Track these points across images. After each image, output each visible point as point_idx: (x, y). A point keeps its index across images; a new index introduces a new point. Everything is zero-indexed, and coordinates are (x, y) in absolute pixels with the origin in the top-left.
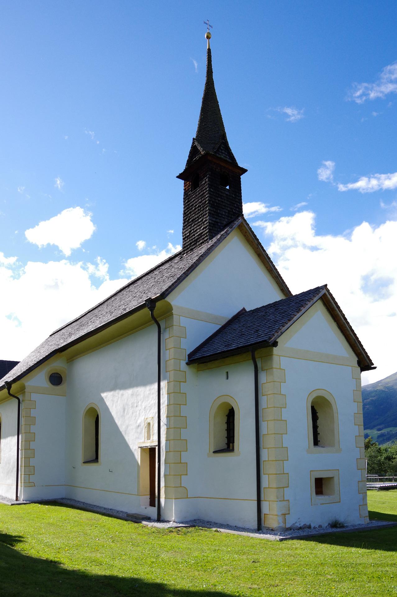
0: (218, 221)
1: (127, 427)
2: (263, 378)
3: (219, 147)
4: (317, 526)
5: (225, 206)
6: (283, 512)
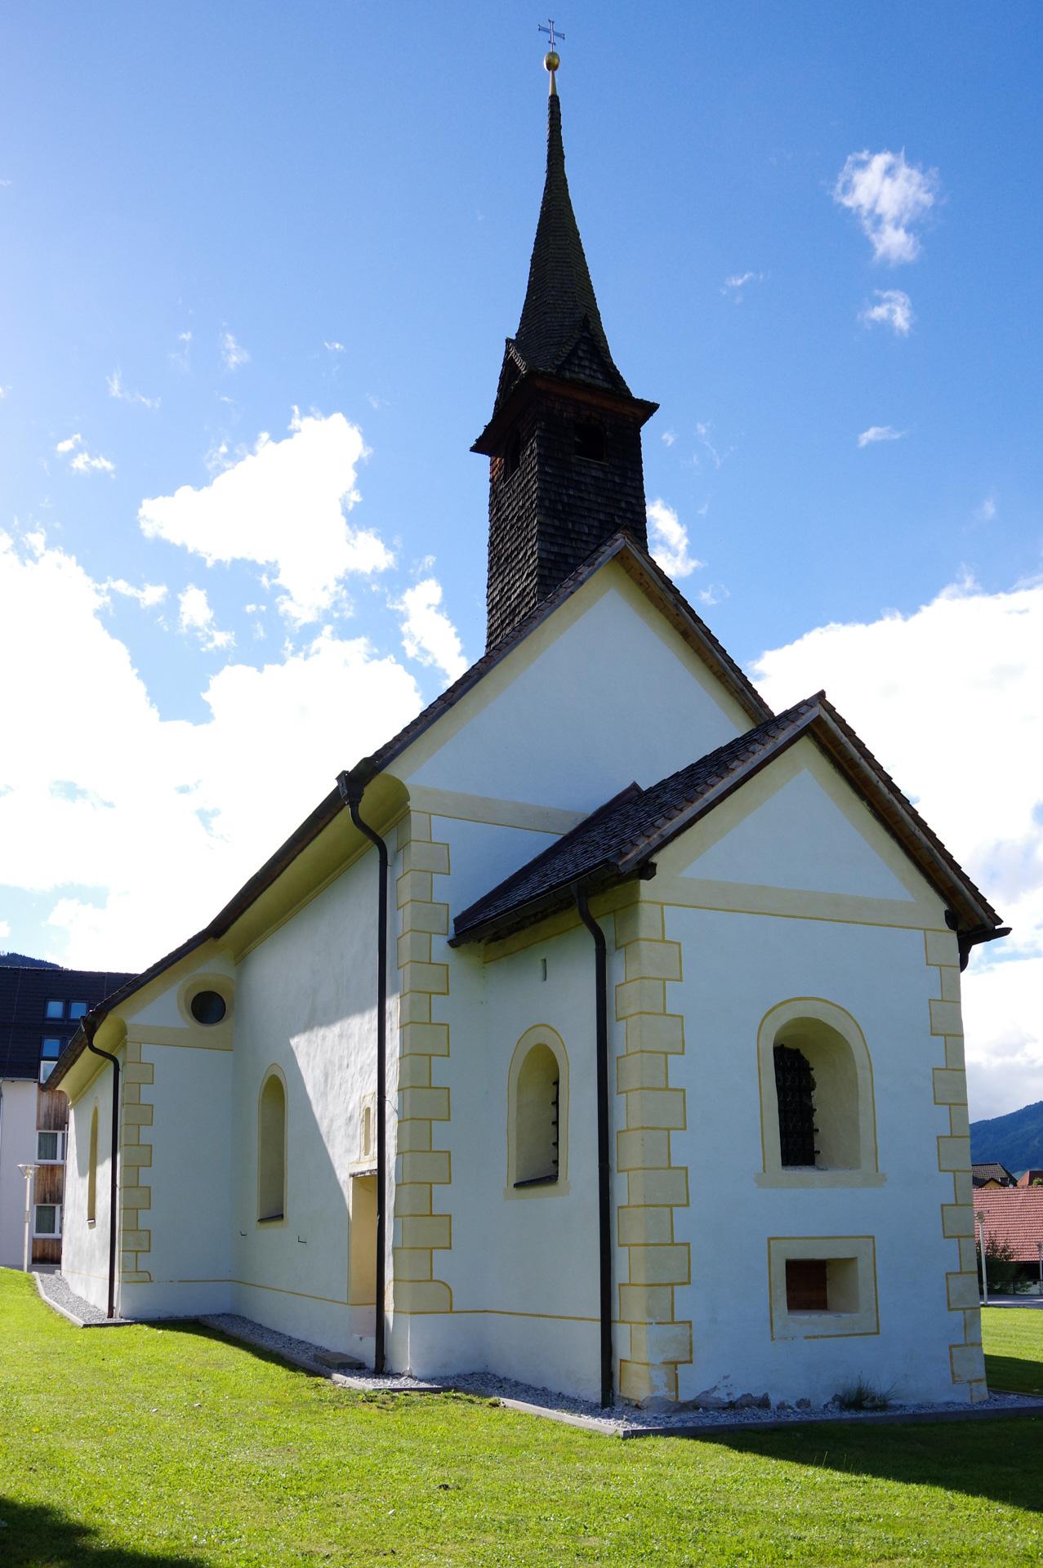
0: (568, 551)
1: (332, 1121)
2: (618, 970)
3: (573, 353)
4: (792, 1403)
5: (589, 510)
6: (671, 1355)
